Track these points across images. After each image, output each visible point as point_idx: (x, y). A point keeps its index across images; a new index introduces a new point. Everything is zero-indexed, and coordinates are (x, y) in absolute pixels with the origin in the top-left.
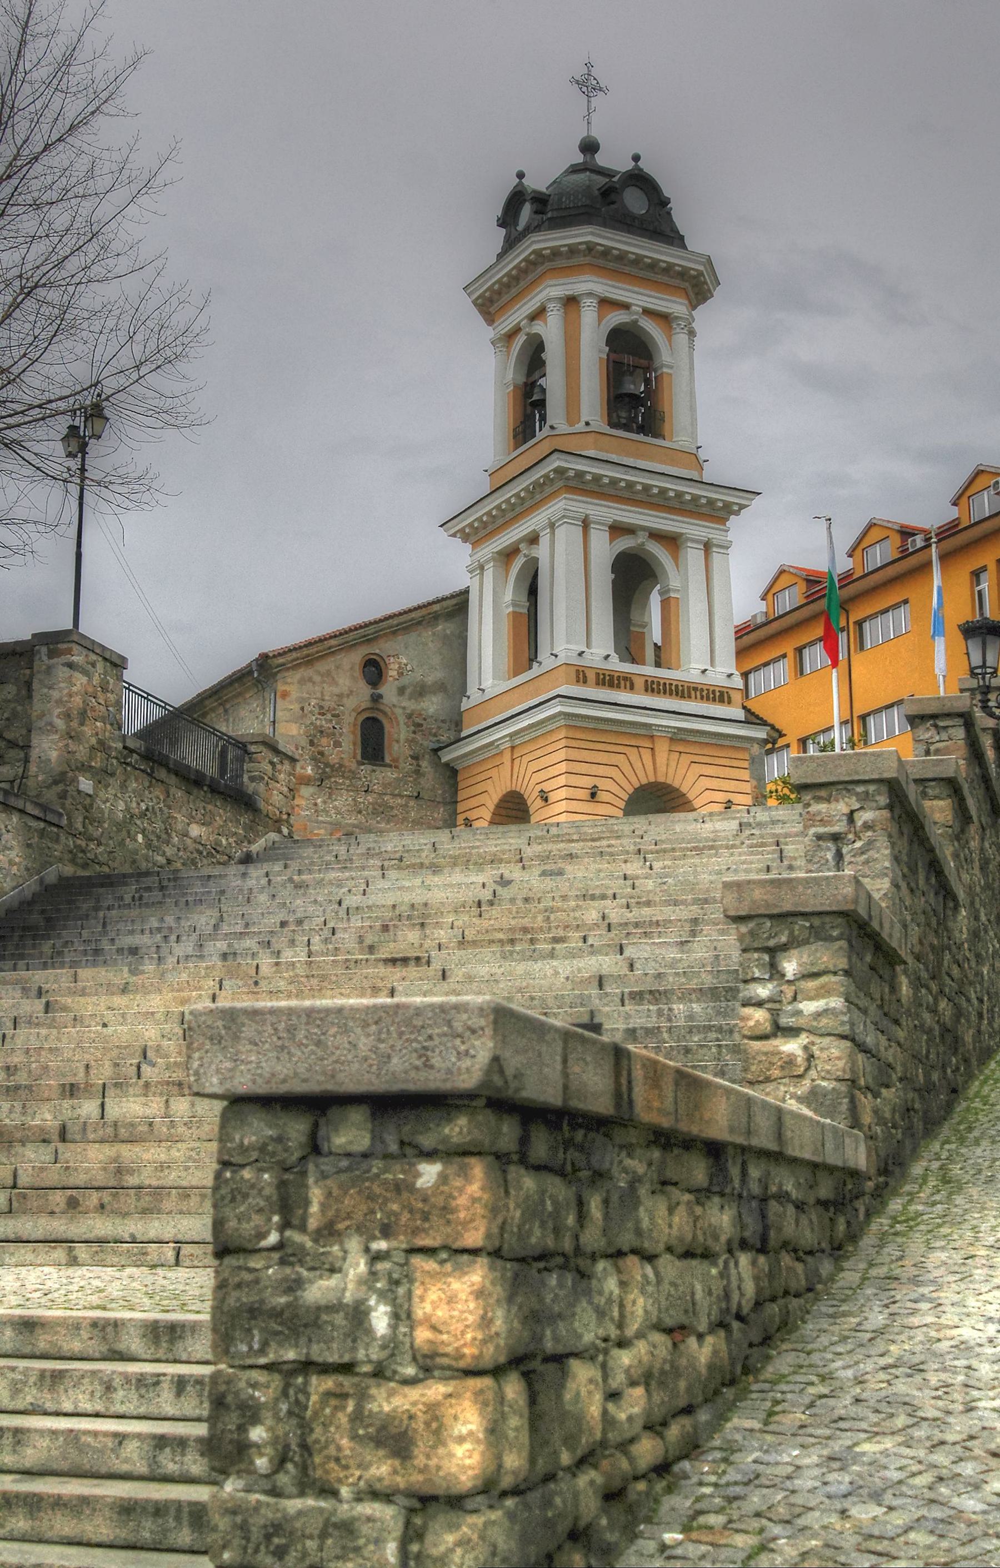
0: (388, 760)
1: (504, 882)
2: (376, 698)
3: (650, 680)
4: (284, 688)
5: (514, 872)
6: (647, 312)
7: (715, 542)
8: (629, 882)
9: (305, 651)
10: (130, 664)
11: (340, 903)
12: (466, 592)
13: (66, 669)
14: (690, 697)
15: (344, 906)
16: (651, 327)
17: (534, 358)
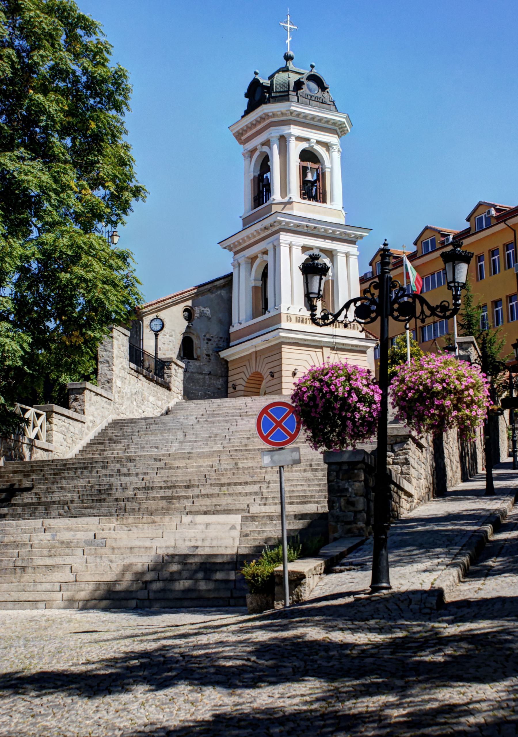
0: (195, 356)
6: (318, 142)
7: (351, 253)
9: (156, 306)
12: (231, 275)
14: (306, 323)
16: (320, 150)
17: (265, 165)
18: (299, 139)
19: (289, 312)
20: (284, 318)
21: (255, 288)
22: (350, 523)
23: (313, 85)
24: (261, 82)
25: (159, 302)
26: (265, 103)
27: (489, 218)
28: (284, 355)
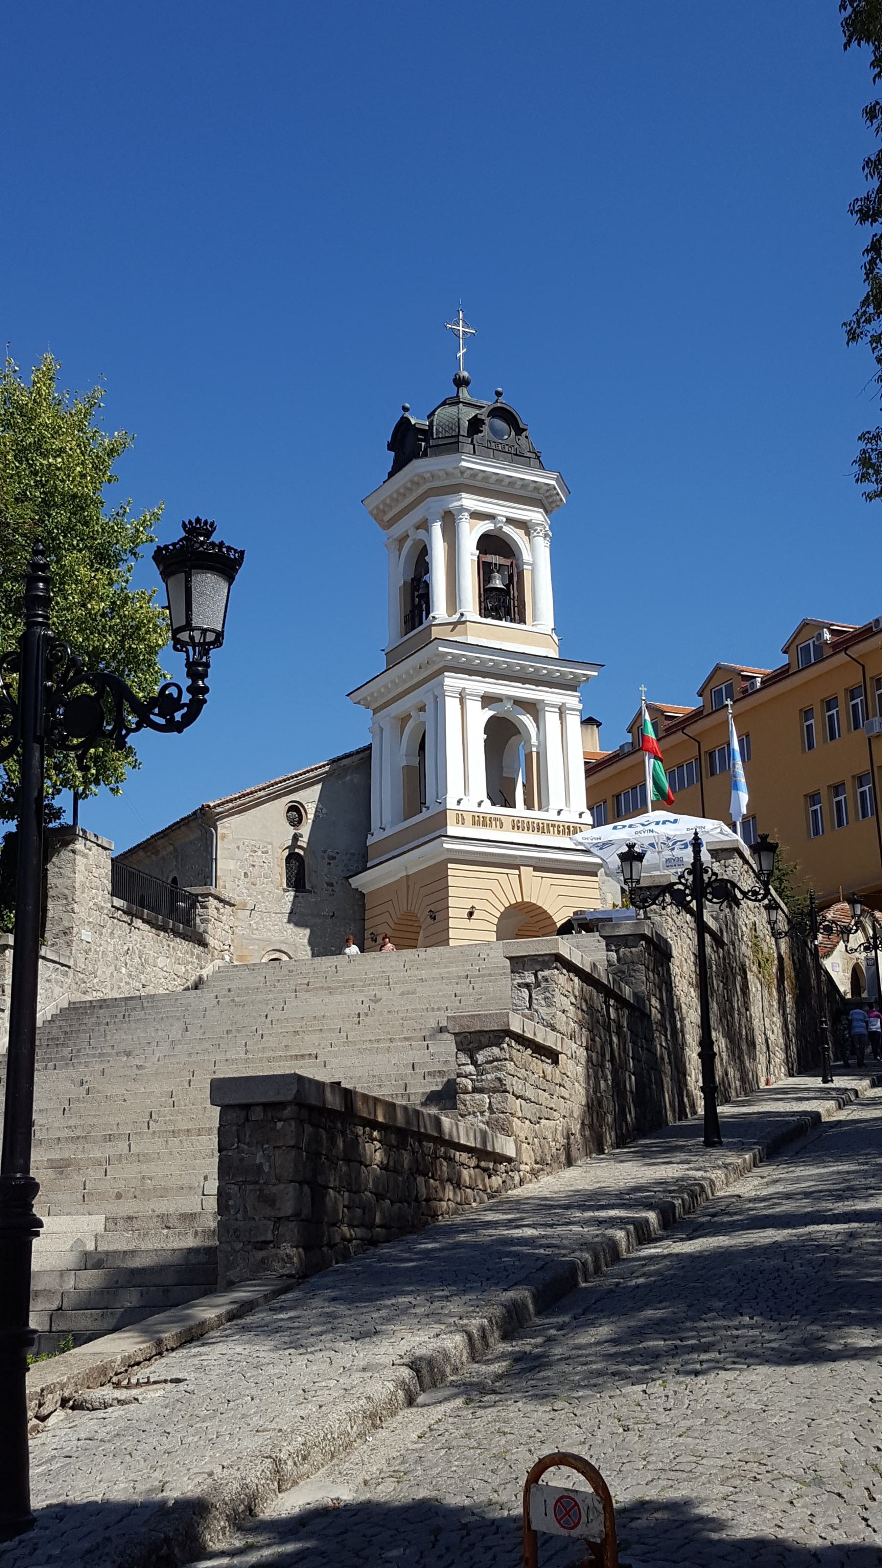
0: (308, 887)
1: (376, 1000)
3: (516, 819)
4: (224, 831)
5: (382, 992)
6: (510, 521)
9: (239, 802)
12: (369, 748)
14: (549, 832)
15: (269, 1019)
16: (516, 535)
18: (477, 515)
19: (462, 807)
20: (451, 817)
21: (407, 768)
22: (263, 1245)
23: (500, 424)
24: (413, 422)
25: (244, 796)
26: (417, 457)
27: (820, 648)
28: (451, 881)
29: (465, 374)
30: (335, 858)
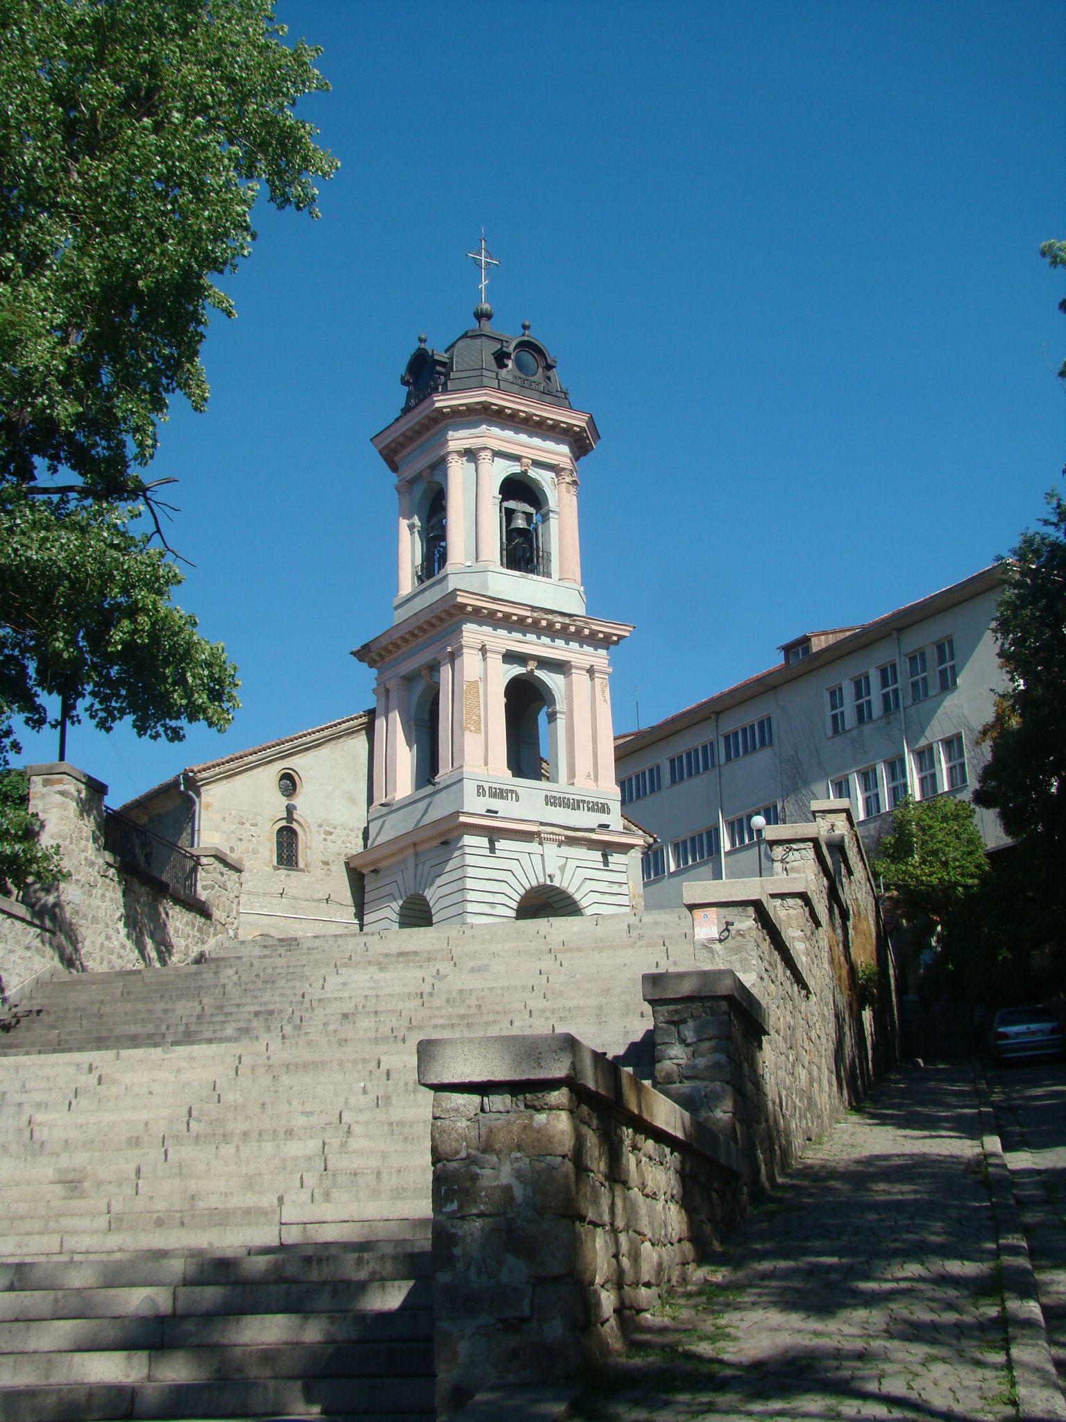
0: (301, 865)
2: (290, 810)
6: (537, 464)
8: (544, 977)
9: (227, 766)
10: (110, 791)
11: (303, 996)
13: (58, 796)
14: (579, 808)
15: (307, 998)
16: (544, 478)
20: (469, 787)
23: (527, 358)
29: (486, 307)
30: (331, 833)
